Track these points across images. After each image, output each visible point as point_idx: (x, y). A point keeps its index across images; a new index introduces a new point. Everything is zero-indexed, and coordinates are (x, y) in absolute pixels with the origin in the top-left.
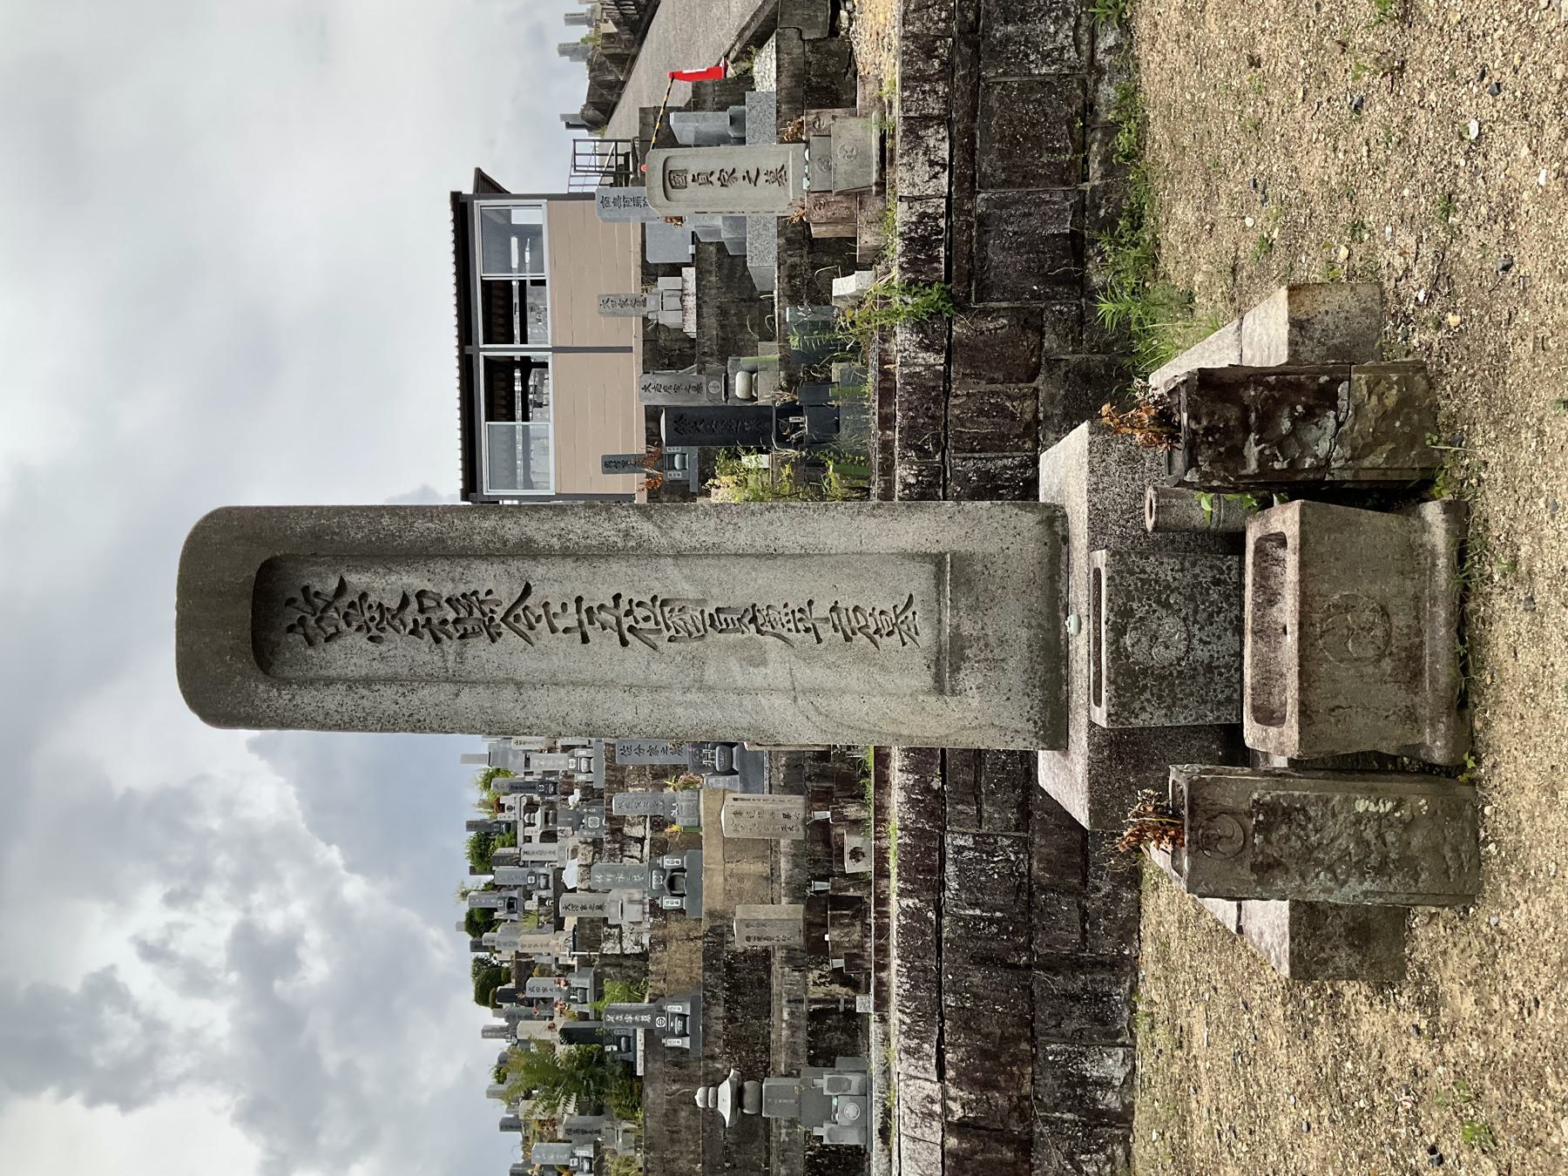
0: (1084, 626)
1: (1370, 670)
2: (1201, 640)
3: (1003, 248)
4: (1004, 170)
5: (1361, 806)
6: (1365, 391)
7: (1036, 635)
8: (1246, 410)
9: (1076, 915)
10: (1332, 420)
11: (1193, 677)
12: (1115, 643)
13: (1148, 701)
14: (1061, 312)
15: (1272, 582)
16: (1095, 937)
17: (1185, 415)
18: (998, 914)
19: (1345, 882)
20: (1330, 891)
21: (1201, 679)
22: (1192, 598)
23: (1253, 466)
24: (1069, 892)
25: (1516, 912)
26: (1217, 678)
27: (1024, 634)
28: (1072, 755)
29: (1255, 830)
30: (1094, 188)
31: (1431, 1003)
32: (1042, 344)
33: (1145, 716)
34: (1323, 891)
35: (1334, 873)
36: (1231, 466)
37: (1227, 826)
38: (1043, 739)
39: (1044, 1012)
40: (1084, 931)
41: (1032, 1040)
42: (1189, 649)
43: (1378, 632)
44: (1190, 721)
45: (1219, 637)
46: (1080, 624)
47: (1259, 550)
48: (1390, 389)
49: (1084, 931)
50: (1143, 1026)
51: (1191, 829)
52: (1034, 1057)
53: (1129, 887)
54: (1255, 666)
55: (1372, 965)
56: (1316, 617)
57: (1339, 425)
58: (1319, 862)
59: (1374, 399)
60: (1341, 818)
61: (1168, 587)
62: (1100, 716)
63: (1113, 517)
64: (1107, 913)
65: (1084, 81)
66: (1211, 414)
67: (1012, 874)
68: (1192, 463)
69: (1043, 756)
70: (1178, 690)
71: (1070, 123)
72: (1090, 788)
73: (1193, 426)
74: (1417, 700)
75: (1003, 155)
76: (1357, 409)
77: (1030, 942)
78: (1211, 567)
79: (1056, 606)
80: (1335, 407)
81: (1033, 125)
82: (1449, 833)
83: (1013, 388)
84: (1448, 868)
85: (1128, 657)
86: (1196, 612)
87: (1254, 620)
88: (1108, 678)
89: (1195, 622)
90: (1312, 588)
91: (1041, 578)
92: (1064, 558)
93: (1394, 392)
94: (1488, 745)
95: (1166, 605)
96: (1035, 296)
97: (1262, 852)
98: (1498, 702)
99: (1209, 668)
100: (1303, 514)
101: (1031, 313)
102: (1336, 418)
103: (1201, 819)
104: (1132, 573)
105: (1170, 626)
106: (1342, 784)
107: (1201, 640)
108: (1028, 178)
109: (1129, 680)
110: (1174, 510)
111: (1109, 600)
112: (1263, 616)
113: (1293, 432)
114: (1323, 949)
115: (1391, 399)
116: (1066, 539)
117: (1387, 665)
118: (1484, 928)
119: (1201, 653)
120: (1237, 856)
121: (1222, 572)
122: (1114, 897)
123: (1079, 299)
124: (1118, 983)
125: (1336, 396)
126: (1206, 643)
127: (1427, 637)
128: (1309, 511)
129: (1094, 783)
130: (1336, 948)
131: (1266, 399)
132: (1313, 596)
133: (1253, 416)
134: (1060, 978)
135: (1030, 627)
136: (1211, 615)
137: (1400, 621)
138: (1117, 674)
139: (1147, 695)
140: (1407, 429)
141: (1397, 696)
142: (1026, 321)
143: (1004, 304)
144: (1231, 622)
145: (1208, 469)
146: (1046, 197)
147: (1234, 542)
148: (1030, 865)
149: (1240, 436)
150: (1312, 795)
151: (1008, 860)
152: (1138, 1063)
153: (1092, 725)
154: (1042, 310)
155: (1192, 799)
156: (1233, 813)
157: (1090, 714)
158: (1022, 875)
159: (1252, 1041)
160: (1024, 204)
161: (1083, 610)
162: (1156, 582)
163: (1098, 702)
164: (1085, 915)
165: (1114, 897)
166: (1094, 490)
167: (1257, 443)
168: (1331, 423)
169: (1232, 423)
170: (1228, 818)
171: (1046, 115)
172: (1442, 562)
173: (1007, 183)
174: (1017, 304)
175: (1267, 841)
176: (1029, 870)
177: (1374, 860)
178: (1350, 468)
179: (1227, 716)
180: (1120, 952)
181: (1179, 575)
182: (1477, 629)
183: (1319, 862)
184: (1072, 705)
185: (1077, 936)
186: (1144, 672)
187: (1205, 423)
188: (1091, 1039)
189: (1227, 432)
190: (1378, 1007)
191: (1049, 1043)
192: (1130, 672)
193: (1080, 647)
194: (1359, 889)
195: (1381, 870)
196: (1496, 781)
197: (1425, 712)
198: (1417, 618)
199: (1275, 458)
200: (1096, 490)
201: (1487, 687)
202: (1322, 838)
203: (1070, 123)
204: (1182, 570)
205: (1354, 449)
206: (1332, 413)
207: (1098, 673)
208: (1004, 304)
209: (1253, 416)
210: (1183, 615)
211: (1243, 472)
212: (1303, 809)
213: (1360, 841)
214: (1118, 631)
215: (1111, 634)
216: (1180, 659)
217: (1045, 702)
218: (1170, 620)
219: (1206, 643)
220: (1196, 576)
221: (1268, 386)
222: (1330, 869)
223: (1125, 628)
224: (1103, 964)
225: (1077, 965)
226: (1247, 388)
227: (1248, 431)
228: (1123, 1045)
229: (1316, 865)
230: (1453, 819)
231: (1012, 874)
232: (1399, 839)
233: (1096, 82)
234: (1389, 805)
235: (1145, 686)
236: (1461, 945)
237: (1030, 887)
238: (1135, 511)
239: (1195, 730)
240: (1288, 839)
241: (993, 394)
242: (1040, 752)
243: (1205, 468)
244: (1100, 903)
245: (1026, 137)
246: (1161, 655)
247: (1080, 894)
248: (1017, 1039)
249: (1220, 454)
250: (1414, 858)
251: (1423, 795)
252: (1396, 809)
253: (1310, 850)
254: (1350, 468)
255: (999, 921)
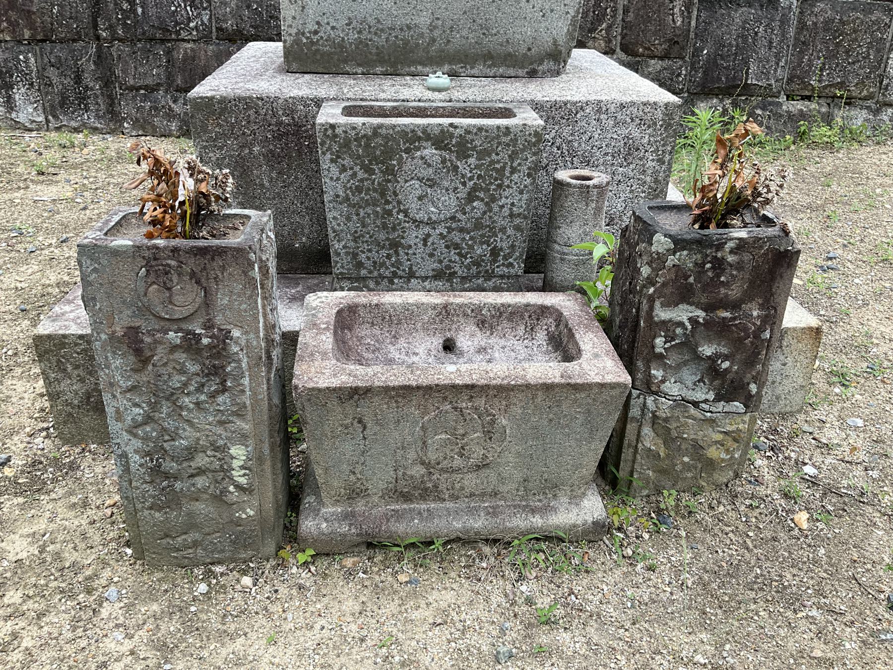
0: (437, 95)
1: (412, 455)
2: (428, 235)
3: (745, 22)
4: (815, 24)
5: (239, 453)
6: (729, 428)
7: (422, 35)
8: (735, 306)
9: (149, 81)
10: (703, 397)
11: (384, 226)
12: (426, 135)
13: (354, 175)
14: (679, 75)
15: (505, 324)
16: (134, 97)
17: (743, 234)
18: (140, 10)
19: (135, 436)
20: (119, 416)
21: (382, 236)
22: (478, 225)
23: (662, 314)
24: (170, 77)
25: (119, 635)
26: (384, 252)
27: (423, 20)
28: (279, 78)
29: (189, 332)
30: (780, 105)
31: (33, 480)
32: (653, 58)
33: (335, 171)
34: (118, 411)
35: (145, 423)
36: (668, 290)
37: (186, 298)
38: (297, 42)
39: (60, 51)
40: (138, 89)
41: (33, 41)
42: (418, 223)
43: (458, 462)
44: (332, 224)
45: (431, 255)
46: (440, 90)
47: (544, 310)
48: (727, 451)
49: (138, 89)
50: (64, 137)
51: (175, 250)
52: (20, 42)
53: (181, 128)
54: (406, 307)
55: (70, 415)
56: (481, 402)
57: (696, 404)
58: (155, 406)
59: (719, 437)
60: (219, 430)
61: (493, 199)
62: (330, 115)
63: (566, 131)
64: (156, 109)
65: (872, 98)
66: (739, 266)
67: (177, 24)
68: (679, 243)
69: (276, 48)
70: (369, 210)
71: (841, 85)
72: (240, 99)
73: (731, 245)
74: (376, 499)
75: (828, 22)
76: (712, 421)
77: (120, 40)
78: (513, 246)
79: (459, 61)
80: (718, 399)
81: (847, 52)
82: (216, 538)
83: (617, 31)
84: (173, 538)
85: (408, 151)
86: (462, 230)
87: (460, 306)
88: (380, 126)
89: (450, 230)
90: (518, 399)
91: (491, 43)
92: (511, 72)
93: (723, 455)
94: (325, 576)
95: (471, 197)
96: (697, 52)
97: (156, 342)
98: (378, 590)
99: (395, 245)
100: (613, 386)
101: (683, 48)
102: (706, 401)
103: (191, 264)
104: (512, 158)
105: (445, 203)
106: (265, 430)
107: (428, 235)
108: (802, 46)
109: (379, 152)
110: (582, 205)
111: (480, 129)
112: (465, 315)
113: (697, 358)
114: (77, 367)
115: (713, 453)
116: (532, 74)
117: (418, 471)
118: (107, 573)
119: (413, 236)
120: (146, 310)
121: (505, 258)
122: (170, 115)
123: (688, 91)
124: (98, 117)
125: (728, 400)
126: (425, 241)
127: (450, 505)
128: (614, 393)
129: (248, 103)
130: (82, 380)
131: (745, 329)
132: (507, 398)
133: (727, 315)
134: (93, 67)
135: (432, 28)
136: (457, 246)
137: (470, 481)
138: (386, 138)
139: (361, 174)
140: (679, 468)
141: (380, 477)
142: (677, 42)
143: (693, 23)
144: (448, 267)
145: (669, 263)
146: (782, 64)
147: (537, 264)
148: (188, 41)
149: (704, 300)
150: (246, 399)
151: (189, 20)
152: (34, 134)
153: (318, 103)
154: (683, 58)
155: (220, 252)
156: (207, 304)
157: (333, 102)
158: (178, 33)
159: (30, 247)
160: (782, 41)
161: (456, 94)
162: (500, 186)
163: (348, 111)
164: (151, 89)
165: (170, 115)
166: (600, 108)
167: (693, 321)
168: (699, 395)
169: (723, 291)
170: (199, 300)
171: (854, 63)
172: (537, 521)
173: (802, 26)
174: (692, 35)
175: (174, 348)
176: (184, 40)
177: (170, 466)
178: (643, 414)
179: (340, 264)
180: (124, 119)
181: (506, 211)
182: (461, 556)
183: (155, 406)
184: (340, 79)
185: (132, 82)
186: (390, 171)
187: (731, 258)
188: (47, 93)
189: (713, 284)
190: (38, 405)
191: (35, 55)
192: (389, 153)
193: (411, 90)
194: (129, 449)
195: (157, 472)
196: (283, 590)
197: (360, 506)
198: (472, 495)
199: (669, 338)
200: (599, 111)
201: (395, 574)
202: (189, 410)
203: (841, 85)
204: (511, 215)
205: (666, 420)
206: (711, 396)
207: (382, 113)
208: (693, 23)
209: (727, 315)
210: (459, 216)
211: (657, 304)
212: (224, 390)
213: (191, 452)
214: (440, 140)
215: (437, 131)
216: (406, 213)
217: (341, 45)
218: (454, 203)
219: (425, 241)
220: (503, 230)
221: (761, 330)
222: (148, 419)
223: (445, 148)
224: (112, 104)
225: (107, 83)
226: (762, 307)
227: (708, 308)
228: (48, 121)
229: (149, 403)
230: (233, 542)
231: (177, 24)
232: (205, 490)
233: (868, 108)
234: (243, 481)
235: (371, 172)
236: (91, 532)
237: (169, 41)
238: (571, 156)
239: (322, 221)
240: (182, 371)
241: (615, 11)
242: (281, 44)
243: (671, 260)
244: (163, 103)
245: (838, 45)
246: (410, 191)
247: (169, 86)
248: (32, 26)
249: (687, 277)
250: (179, 505)
251: (260, 511)
252: (238, 487)
253: (171, 397)
254: (643, 414)
255: (134, 11)
